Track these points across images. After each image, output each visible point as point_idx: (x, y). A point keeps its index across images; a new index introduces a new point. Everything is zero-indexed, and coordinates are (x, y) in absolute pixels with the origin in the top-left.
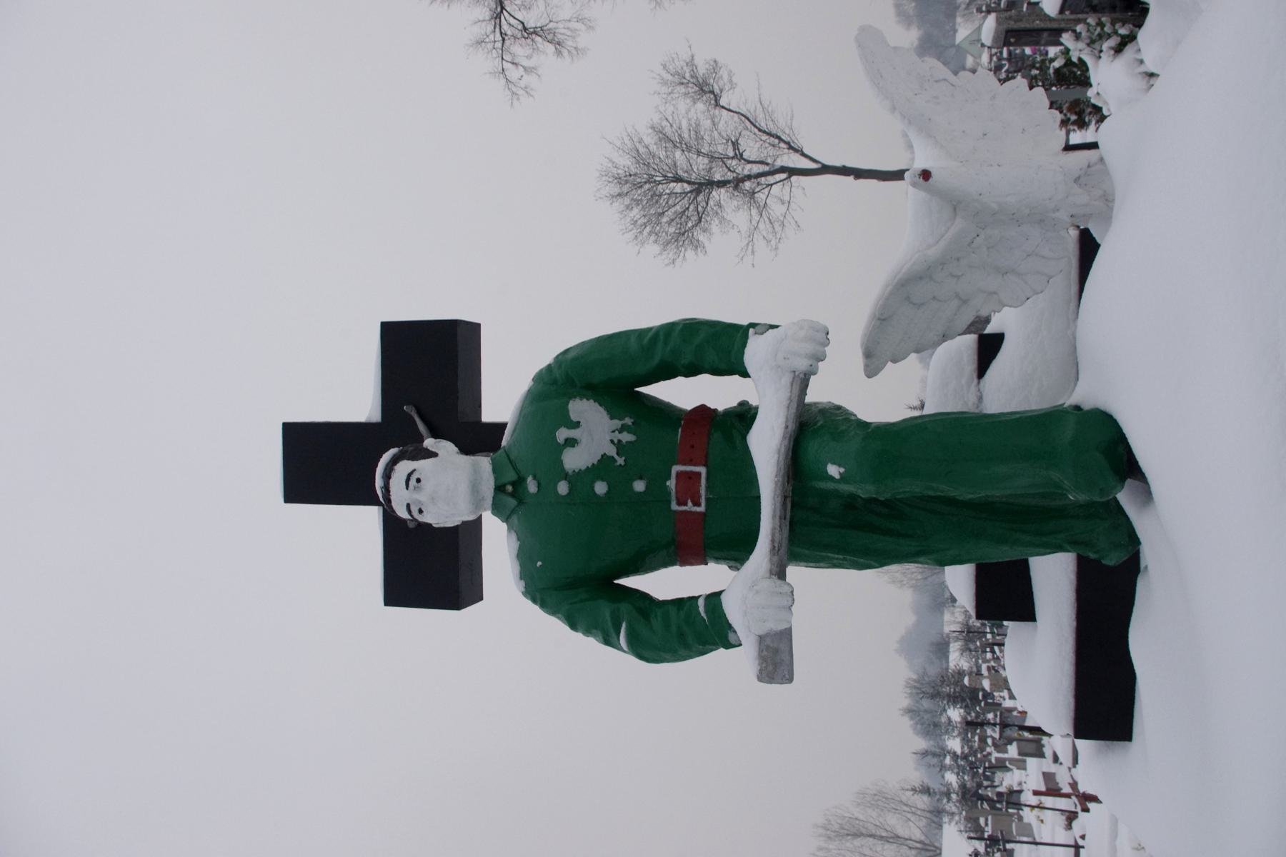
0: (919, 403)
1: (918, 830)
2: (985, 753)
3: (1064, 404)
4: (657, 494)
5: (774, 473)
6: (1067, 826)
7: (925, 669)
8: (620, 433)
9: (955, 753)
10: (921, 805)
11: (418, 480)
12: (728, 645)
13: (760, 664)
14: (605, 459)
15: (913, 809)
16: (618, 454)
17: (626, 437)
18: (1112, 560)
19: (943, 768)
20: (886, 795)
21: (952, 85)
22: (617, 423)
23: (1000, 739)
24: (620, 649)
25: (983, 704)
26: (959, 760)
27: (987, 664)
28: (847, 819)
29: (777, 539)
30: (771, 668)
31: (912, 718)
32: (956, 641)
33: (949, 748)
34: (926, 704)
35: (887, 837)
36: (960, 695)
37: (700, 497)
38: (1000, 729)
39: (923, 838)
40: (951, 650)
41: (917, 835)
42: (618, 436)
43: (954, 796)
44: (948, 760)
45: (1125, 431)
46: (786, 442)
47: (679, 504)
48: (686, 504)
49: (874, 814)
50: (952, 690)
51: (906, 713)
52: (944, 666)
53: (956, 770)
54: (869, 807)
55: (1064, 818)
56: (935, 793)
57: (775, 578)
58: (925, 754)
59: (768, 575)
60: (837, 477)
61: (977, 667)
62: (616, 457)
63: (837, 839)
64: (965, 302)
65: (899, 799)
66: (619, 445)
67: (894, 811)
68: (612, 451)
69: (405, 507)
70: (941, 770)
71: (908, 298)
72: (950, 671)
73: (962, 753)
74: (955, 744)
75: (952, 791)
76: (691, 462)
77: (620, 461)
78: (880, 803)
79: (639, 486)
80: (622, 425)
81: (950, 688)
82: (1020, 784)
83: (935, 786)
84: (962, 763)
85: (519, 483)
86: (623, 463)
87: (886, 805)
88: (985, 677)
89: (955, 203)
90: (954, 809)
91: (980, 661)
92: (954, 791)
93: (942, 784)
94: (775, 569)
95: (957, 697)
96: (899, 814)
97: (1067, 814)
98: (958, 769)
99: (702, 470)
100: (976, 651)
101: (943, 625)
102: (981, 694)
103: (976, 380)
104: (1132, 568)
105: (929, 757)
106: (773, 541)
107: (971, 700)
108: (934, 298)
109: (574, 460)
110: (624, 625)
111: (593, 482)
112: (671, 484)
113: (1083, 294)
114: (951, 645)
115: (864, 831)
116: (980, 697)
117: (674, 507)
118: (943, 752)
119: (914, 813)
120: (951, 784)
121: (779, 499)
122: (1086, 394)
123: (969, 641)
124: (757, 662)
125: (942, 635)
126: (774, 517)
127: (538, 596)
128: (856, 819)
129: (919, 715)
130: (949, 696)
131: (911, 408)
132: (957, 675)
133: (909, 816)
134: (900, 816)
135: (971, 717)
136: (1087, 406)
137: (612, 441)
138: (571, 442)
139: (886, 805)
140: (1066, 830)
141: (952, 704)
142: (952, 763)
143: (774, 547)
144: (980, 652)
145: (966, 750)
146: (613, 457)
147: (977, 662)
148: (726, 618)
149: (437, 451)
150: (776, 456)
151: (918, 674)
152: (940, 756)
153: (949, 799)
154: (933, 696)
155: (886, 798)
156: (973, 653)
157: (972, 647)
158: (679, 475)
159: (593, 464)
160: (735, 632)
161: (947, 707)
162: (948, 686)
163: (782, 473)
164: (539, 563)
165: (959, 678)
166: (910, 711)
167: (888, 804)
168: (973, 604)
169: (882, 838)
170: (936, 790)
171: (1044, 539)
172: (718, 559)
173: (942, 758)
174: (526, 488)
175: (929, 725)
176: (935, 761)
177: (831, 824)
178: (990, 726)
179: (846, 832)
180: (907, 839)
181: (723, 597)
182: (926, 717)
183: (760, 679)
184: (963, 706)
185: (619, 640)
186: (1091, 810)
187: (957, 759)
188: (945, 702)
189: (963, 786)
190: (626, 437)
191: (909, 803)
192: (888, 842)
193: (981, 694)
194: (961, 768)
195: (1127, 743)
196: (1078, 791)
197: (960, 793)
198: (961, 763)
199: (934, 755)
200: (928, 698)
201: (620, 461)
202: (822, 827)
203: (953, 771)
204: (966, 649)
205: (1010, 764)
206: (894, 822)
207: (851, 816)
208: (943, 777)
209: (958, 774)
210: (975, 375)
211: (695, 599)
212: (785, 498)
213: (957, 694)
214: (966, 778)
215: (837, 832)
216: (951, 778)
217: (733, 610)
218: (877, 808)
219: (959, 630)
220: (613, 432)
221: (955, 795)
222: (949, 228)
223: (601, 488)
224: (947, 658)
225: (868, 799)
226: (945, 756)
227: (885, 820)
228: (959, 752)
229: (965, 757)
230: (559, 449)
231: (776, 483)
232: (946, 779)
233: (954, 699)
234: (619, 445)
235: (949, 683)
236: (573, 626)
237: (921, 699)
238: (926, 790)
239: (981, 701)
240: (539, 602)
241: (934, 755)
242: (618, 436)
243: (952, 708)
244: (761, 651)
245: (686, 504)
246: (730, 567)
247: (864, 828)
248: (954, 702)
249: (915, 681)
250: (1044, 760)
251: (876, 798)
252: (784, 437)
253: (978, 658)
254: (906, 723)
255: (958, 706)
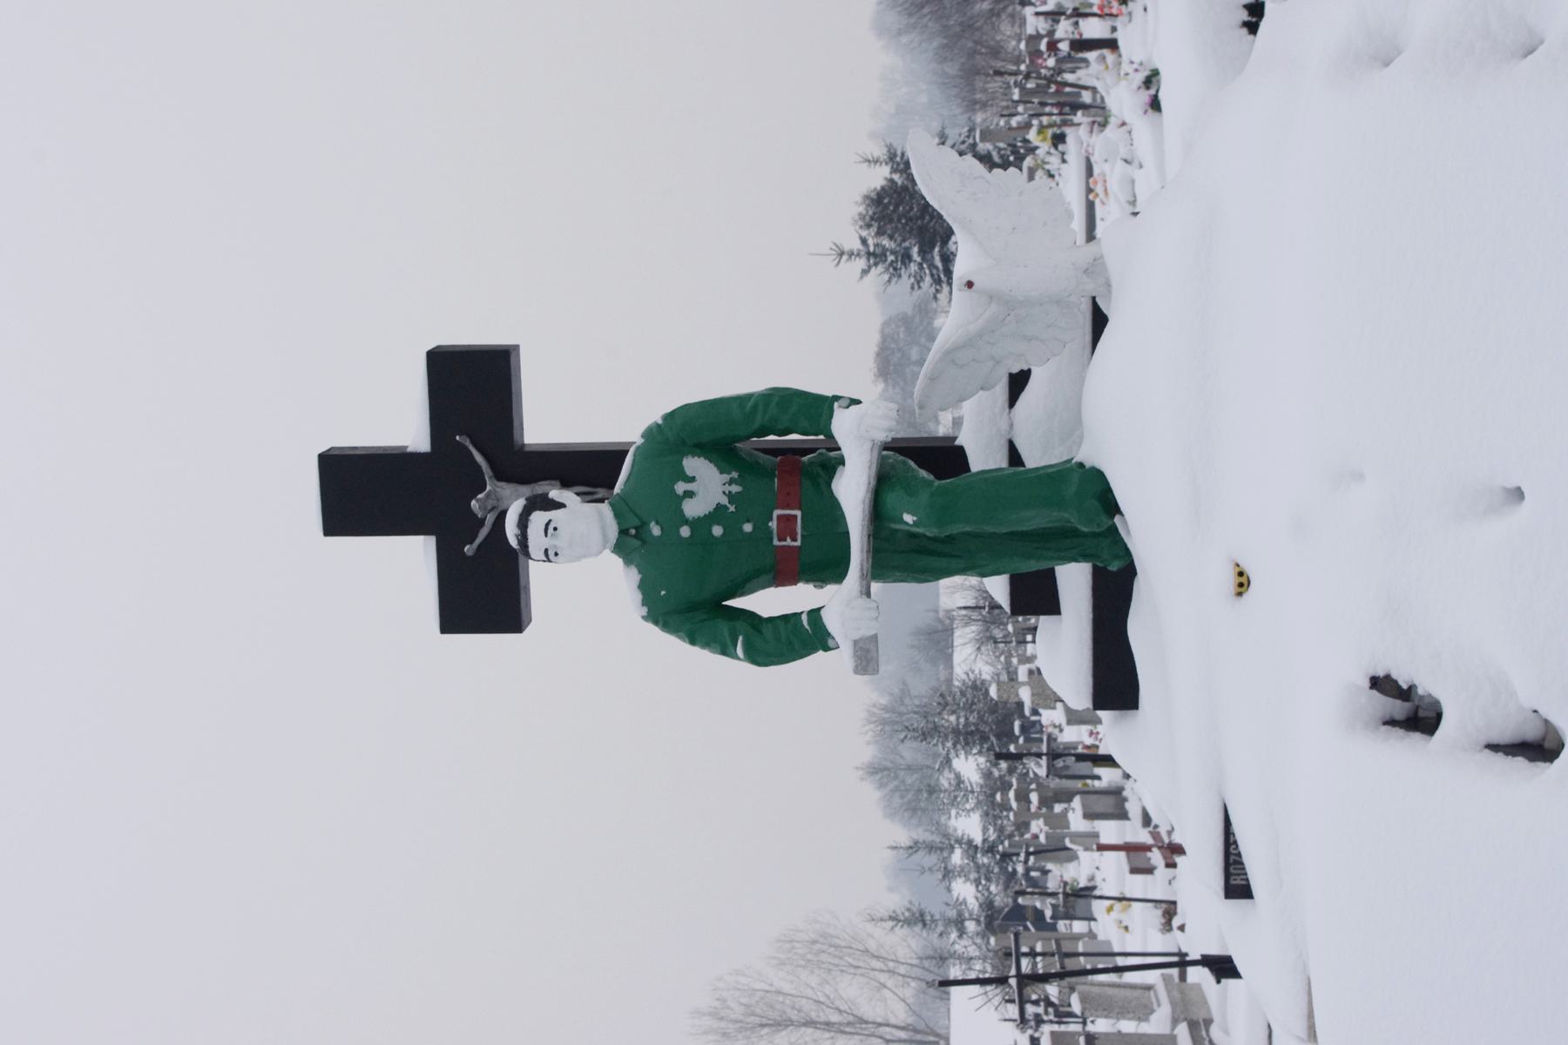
0: (885, 150)
1: (902, 1003)
2: (1027, 836)
3: (1072, 459)
4: (763, 532)
5: (861, 518)
6: (1164, 925)
7: (904, 683)
8: (730, 485)
9: (970, 842)
10: (903, 953)
11: (555, 529)
12: (827, 649)
13: (856, 661)
14: (719, 507)
15: (891, 964)
16: (729, 503)
17: (735, 489)
18: (1114, 567)
19: (948, 874)
20: (837, 941)
21: (987, 182)
22: (726, 477)
23: (1047, 776)
24: (739, 659)
25: (1021, 740)
26: (979, 855)
27: (1028, 666)
28: (759, 994)
29: (865, 568)
30: (864, 663)
31: (881, 785)
32: (967, 624)
33: (960, 833)
34: (911, 752)
35: (840, 1024)
36: (977, 730)
37: (796, 534)
38: (1048, 760)
39: (910, 1020)
40: (955, 644)
41: (900, 1014)
42: (728, 488)
43: (971, 926)
44: (957, 858)
45: (1112, 485)
46: (869, 495)
47: (780, 540)
48: (785, 540)
49: (814, 980)
50: (962, 720)
51: (872, 774)
52: (943, 675)
53: (973, 876)
54: (804, 967)
55: (1159, 912)
56: (933, 921)
57: (864, 597)
58: (914, 847)
59: (859, 594)
60: (911, 523)
61: (1008, 672)
62: (728, 505)
63: (740, 1036)
64: (998, 362)
65: (861, 948)
66: (730, 495)
67: (852, 971)
68: (725, 501)
69: (543, 551)
70: (944, 877)
71: (953, 361)
72: (956, 683)
73: (985, 840)
74: (970, 825)
75: (967, 915)
76: (788, 507)
77: (732, 509)
78: (824, 957)
79: (748, 528)
80: (731, 478)
81: (958, 719)
82: (1092, 878)
83: (935, 908)
84: (986, 860)
85: (642, 528)
86: (734, 510)
87: (836, 961)
88: (1023, 684)
89: (992, 297)
90: (973, 951)
91: (1015, 661)
92: (971, 915)
93: (947, 904)
94: (864, 590)
95: (972, 733)
96: (862, 975)
97: (1164, 905)
98: (978, 872)
99: (798, 513)
100: (1005, 642)
101: (938, 595)
102: (1017, 724)
103: (1007, 410)
104: (1129, 572)
105: (921, 853)
106: (862, 569)
107: (998, 737)
108: (973, 360)
109: (692, 509)
110: (741, 638)
111: (711, 526)
112: (773, 524)
113: (1096, 351)
114: (957, 633)
115: (794, 1015)
116: (1017, 731)
117: (776, 542)
118: (947, 843)
119: (892, 972)
120: (965, 902)
121: (866, 538)
122: (1088, 455)
123: (993, 623)
124: (852, 660)
125: (937, 612)
126: (862, 551)
127: (660, 619)
128: (779, 992)
129: (896, 777)
130: (956, 732)
131: (869, 161)
132: (970, 690)
133: (883, 977)
134: (865, 980)
135: (1000, 770)
136: (1088, 465)
137: (724, 493)
138: (690, 494)
139: (836, 961)
140: (1163, 933)
141: (963, 748)
142: (966, 861)
143: (863, 575)
144: (1014, 644)
145: (992, 835)
146: (726, 506)
147: (1008, 663)
148: (827, 630)
149: (564, 502)
150: (862, 506)
151: (891, 694)
152: (942, 850)
153: (962, 932)
154: (925, 736)
155: (837, 947)
156: (1001, 645)
157: (998, 634)
158: (779, 517)
159: (710, 512)
160: (833, 638)
161: (952, 754)
162: (953, 712)
163: (867, 519)
164: (663, 593)
165: (974, 696)
166: (876, 771)
167: (841, 958)
168: (1008, 602)
169: (828, 1025)
170: (937, 917)
171: (1062, 554)
172: (807, 581)
173: (945, 854)
174: (650, 532)
175: (920, 791)
176: (932, 859)
177: (728, 1008)
178: (1032, 758)
179: (757, 1020)
180: (880, 1025)
181: (823, 612)
182: (910, 780)
183: (857, 671)
184: (984, 750)
185: (736, 650)
186: (1179, 866)
187: (976, 853)
188: (949, 744)
189: (988, 905)
190: (735, 489)
191: (884, 954)
192: (843, 1032)
193: (1017, 724)
194: (983, 871)
195: (1135, 711)
196: (1162, 841)
197: (982, 919)
198: (984, 860)
199: (931, 848)
200: (915, 738)
201: (732, 509)
202: (710, 1014)
203: (967, 879)
204: (986, 639)
205: (1072, 842)
206: (855, 994)
207: (767, 988)
208: (949, 890)
209: (977, 882)
210: (1007, 405)
211: (797, 615)
212: (869, 536)
213: (973, 728)
214: (993, 888)
215: (741, 1021)
216: (965, 891)
217: (831, 621)
218: (820, 968)
219: (971, 603)
220: (724, 484)
221: (974, 923)
222: (985, 311)
223: (717, 531)
224: (949, 660)
225: (800, 951)
226: (952, 848)
227: (836, 990)
228: (978, 839)
229: (990, 849)
230: (680, 499)
231: (863, 526)
232: (955, 894)
233: (967, 738)
234: (730, 495)
235: (955, 708)
236: (693, 642)
237: (902, 741)
238: (919, 919)
239: (1018, 738)
240: (661, 623)
241: (931, 848)
242: (728, 488)
243: (962, 756)
244: (855, 651)
245: (785, 540)
246: (815, 586)
247: (793, 1008)
248: (967, 744)
249: (885, 709)
250: (1127, 822)
251: (818, 946)
252: (867, 491)
253: (1011, 655)
254: (870, 795)
255: (975, 751)
